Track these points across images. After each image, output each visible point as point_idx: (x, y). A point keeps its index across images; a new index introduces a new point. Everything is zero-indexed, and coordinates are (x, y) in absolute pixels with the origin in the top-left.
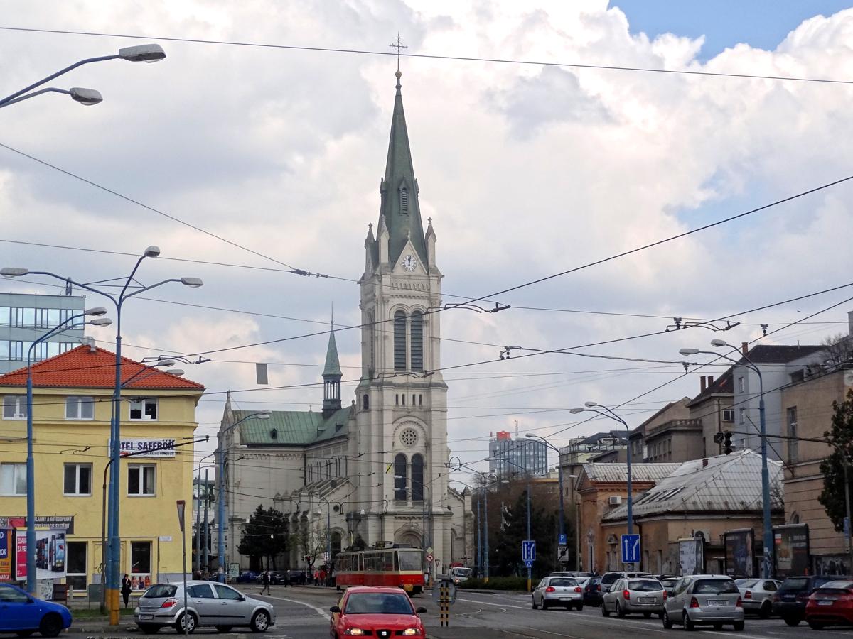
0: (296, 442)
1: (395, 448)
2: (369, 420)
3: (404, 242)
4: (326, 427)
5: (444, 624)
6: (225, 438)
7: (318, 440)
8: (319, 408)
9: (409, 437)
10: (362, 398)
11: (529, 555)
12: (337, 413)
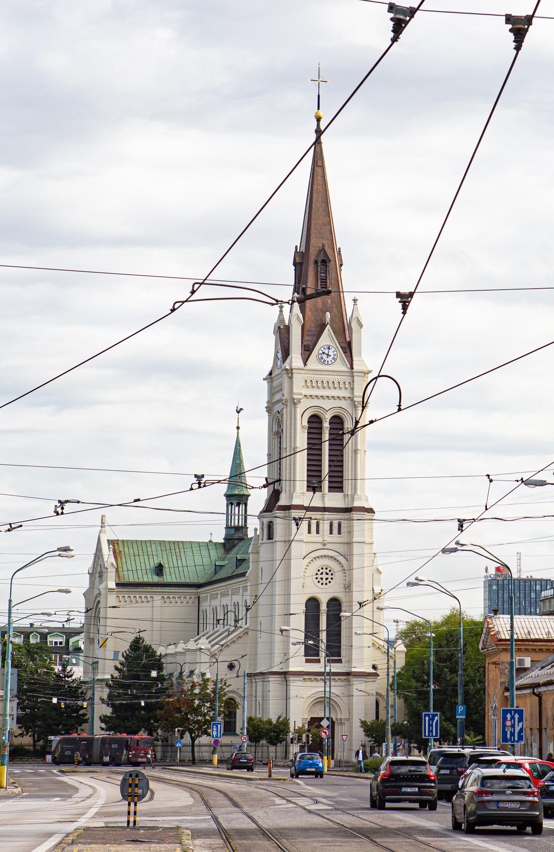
0: (188, 581)
1: (488, 574)
2: (273, 552)
3: (323, 327)
4: (226, 562)
5: (131, 824)
6: (97, 575)
7: (215, 578)
8: (219, 537)
9: (324, 576)
10: (265, 526)
11: (430, 731)
12: (241, 544)
